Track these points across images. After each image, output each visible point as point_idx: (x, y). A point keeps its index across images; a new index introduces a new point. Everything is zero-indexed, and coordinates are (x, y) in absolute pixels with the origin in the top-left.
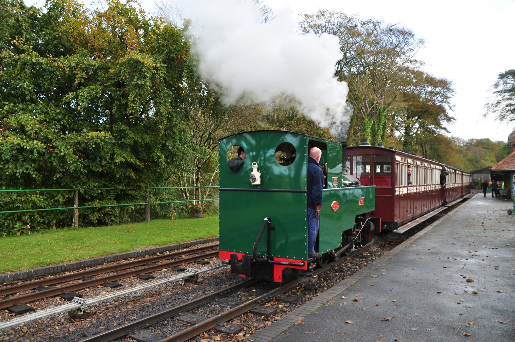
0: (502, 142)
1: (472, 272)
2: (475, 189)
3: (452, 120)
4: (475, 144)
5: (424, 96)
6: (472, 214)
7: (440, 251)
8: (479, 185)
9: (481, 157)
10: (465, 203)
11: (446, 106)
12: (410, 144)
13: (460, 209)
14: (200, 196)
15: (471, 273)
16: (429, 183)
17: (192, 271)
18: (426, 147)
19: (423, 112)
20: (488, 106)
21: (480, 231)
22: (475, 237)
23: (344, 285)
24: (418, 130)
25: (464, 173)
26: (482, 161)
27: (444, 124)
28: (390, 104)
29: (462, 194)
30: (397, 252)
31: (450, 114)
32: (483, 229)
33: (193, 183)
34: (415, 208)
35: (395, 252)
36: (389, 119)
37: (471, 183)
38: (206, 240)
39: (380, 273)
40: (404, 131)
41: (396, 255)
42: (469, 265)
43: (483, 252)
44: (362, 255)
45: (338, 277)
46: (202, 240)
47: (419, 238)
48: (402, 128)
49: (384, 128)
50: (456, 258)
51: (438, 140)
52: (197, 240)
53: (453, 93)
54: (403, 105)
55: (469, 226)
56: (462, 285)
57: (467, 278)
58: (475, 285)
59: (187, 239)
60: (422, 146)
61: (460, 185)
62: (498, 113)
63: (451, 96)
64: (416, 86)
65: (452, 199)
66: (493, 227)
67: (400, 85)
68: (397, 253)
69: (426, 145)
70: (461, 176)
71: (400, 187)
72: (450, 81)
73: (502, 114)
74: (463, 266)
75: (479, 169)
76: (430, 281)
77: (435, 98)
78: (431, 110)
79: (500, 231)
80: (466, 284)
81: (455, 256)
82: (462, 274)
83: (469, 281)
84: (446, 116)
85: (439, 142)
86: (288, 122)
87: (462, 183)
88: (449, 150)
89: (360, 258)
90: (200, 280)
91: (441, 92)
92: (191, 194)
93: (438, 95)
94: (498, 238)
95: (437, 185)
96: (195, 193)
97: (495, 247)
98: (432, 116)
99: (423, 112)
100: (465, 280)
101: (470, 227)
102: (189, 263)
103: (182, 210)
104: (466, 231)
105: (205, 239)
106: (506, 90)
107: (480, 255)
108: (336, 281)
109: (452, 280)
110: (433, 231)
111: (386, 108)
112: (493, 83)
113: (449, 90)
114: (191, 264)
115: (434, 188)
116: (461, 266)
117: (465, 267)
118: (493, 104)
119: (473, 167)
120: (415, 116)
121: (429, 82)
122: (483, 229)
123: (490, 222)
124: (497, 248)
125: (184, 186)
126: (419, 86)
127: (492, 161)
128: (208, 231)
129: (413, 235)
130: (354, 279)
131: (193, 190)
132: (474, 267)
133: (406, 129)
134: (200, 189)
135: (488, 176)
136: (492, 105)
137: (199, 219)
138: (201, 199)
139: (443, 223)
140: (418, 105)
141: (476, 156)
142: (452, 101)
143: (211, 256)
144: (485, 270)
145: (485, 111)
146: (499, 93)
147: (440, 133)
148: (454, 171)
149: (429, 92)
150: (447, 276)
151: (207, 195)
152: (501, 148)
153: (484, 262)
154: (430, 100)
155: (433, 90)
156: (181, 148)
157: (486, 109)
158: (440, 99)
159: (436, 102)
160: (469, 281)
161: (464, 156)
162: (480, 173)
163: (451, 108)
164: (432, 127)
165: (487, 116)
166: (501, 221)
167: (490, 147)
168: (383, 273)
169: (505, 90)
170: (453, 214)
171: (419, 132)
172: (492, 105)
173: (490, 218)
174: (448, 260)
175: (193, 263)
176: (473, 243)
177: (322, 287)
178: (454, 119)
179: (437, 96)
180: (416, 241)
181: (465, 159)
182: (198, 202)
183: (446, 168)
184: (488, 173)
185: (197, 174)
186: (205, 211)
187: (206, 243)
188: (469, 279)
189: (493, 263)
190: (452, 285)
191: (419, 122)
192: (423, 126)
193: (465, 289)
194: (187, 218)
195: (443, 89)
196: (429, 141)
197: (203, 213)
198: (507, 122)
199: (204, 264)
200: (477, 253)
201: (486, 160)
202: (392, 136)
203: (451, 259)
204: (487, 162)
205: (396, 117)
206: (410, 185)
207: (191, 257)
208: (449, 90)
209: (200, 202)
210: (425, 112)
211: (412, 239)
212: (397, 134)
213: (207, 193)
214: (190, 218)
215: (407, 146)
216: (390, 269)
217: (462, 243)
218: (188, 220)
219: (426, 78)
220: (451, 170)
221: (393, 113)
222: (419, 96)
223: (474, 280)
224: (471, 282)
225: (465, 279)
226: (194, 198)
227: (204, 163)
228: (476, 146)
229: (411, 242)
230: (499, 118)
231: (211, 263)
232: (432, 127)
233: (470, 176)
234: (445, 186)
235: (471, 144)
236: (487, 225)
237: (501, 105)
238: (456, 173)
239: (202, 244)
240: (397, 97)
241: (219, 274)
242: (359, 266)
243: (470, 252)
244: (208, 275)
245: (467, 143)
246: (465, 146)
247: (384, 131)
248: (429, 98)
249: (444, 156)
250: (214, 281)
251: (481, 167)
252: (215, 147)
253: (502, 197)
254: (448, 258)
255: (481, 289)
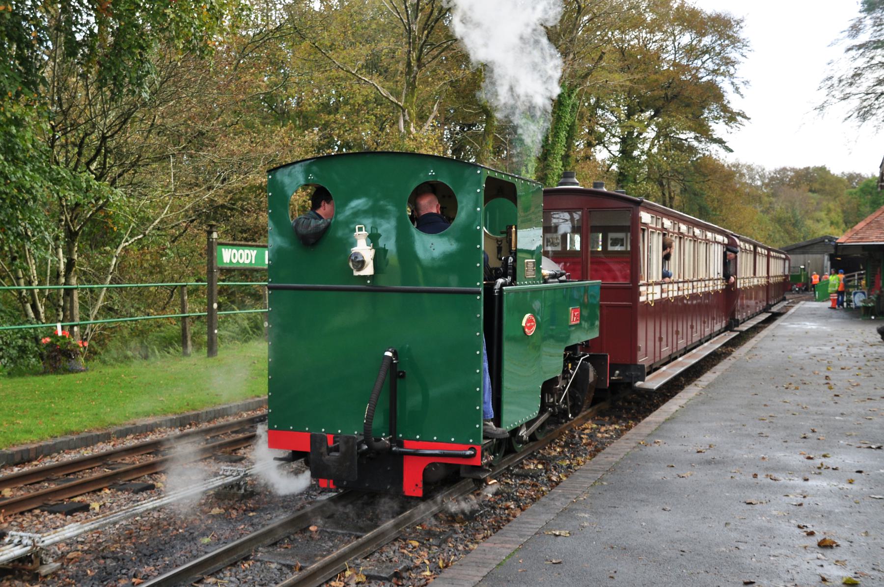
0: (859, 175)
1: (826, 515)
2: (791, 290)
3: (739, 118)
4: (791, 180)
5: (672, 57)
6: (795, 354)
7: (730, 454)
8: (800, 280)
9: (807, 212)
10: (772, 326)
11: (724, 83)
12: (632, 179)
13: (762, 340)
14: (76, 310)
15: (824, 521)
16: (702, 275)
17: (25, 542)
18: (673, 189)
19: (668, 99)
20: (829, 83)
21: (823, 399)
22: (816, 417)
23: (479, 564)
24: (653, 145)
25: (772, 253)
26: (809, 222)
27: (719, 129)
28: (587, 75)
29: (767, 304)
30: (616, 459)
31: (734, 103)
32: (831, 393)
33: (58, 276)
34: (657, 339)
35: (610, 459)
36: (582, 116)
37: (786, 276)
38: (87, 438)
39: (575, 523)
40: (618, 147)
41: (613, 469)
42: (813, 495)
43: (843, 457)
44: (523, 468)
45: (461, 536)
46: (74, 437)
47: (671, 419)
48: (613, 140)
49: (570, 138)
50: (775, 475)
51: (703, 170)
52: (59, 439)
53: (745, 51)
54: (619, 79)
55: (793, 387)
56: (809, 556)
57: (819, 537)
58: (845, 557)
59: (28, 436)
60: (661, 184)
61: (763, 281)
62: (855, 102)
63: (740, 58)
64: (652, 32)
65: (747, 313)
66: (856, 389)
67: (612, 26)
68: (617, 463)
69: (672, 183)
70: (765, 260)
71: (648, 285)
72: (737, 17)
73: (865, 104)
74: (800, 499)
75: (802, 242)
76: (717, 545)
77: (698, 63)
78: (686, 94)
79: (878, 398)
80: (820, 556)
81: (774, 469)
82: (802, 524)
83: (824, 545)
84: (725, 109)
85: (704, 175)
86: (325, 117)
87: (768, 277)
88: (729, 195)
89: (518, 476)
90: (52, 565)
91: (714, 48)
92: (52, 301)
93: (707, 56)
94: (875, 419)
95: (718, 279)
96: (62, 303)
97: (874, 442)
98: (688, 110)
99: (668, 99)
100: (813, 542)
101: (797, 388)
102: (22, 513)
103: (23, 350)
104: (788, 398)
105: (83, 435)
106: (879, 41)
107: (837, 466)
108: (456, 547)
109: (777, 540)
110: (702, 401)
111: (576, 87)
112: (848, 25)
113: (733, 43)
114: (28, 515)
115: (711, 287)
116: (795, 499)
117: (805, 501)
118: (843, 77)
119: (787, 239)
120: (648, 108)
121: (686, 20)
122: (831, 393)
123: (845, 374)
124: (879, 448)
125: (30, 283)
126: (660, 30)
127: (832, 223)
128: (95, 411)
129: (651, 412)
130: (506, 542)
131: (58, 294)
132: (830, 500)
133: (624, 141)
134: (76, 293)
135: (823, 261)
136: (840, 81)
137: (71, 376)
138: (81, 319)
139: (723, 379)
140: (657, 80)
141: (793, 210)
142: (741, 71)
143: (95, 486)
144: (862, 510)
145: (821, 97)
146: (861, 51)
147: (707, 153)
148: (752, 247)
149: (683, 48)
150: (760, 529)
151: (97, 308)
152: (854, 190)
153: (855, 487)
154: (685, 69)
155: (694, 43)
156: (14, 173)
157: (825, 91)
158: (710, 65)
159: (702, 73)
160: (824, 545)
161: (766, 211)
162: (803, 253)
163: (737, 89)
164: (688, 136)
165: (825, 110)
166: (873, 373)
167: (827, 187)
168: (586, 524)
169: (875, 42)
170: (747, 354)
171: (655, 150)
172: (840, 81)
173: (843, 364)
174: (755, 480)
175: (37, 512)
176: (813, 431)
177: (417, 567)
178: (745, 117)
179: (705, 58)
180: (661, 426)
181: (766, 218)
182: (72, 327)
183: (737, 241)
184: (823, 253)
185: (68, 252)
186: (92, 354)
187: (87, 446)
188: (824, 540)
189: (878, 489)
190: (781, 559)
191: (657, 125)
192: (666, 136)
193: (820, 571)
194: (37, 373)
195: (720, 39)
196: (679, 173)
197: (86, 359)
198: (876, 123)
199: (71, 511)
200: (830, 462)
201: (818, 221)
202: (587, 157)
203: (761, 477)
204: (820, 225)
205: (600, 112)
206: (667, 279)
207: (32, 493)
208: (734, 41)
209: (76, 329)
210: (672, 98)
211: (649, 422)
212: (601, 154)
213: (100, 304)
214: (45, 373)
215: (625, 183)
216: (601, 510)
217: (783, 434)
218: (39, 379)
219: (677, 9)
220: (747, 245)
221: (592, 101)
222: (657, 57)
223: (839, 543)
224: (831, 547)
225: (811, 538)
226: (61, 317)
227: (88, 220)
228: (794, 187)
229: (648, 431)
230: (856, 114)
231: (95, 506)
232: (688, 136)
233: (784, 260)
234: (735, 283)
235: (782, 180)
236: (839, 384)
237: (862, 79)
238: (755, 253)
239: (75, 448)
240: (605, 57)
241: (116, 542)
242: (517, 500)
243: (809, 458)
244: (80, 547)
245: (772, 179)
246: (767, 185)
247: (569, 145)
248: (684, 62)
249: (715, 209)
250: (95, 564)
251: (804, 238)
252: (120, 175)
253: (862, 311)
254: (755, 476)
255: (866, 572)
